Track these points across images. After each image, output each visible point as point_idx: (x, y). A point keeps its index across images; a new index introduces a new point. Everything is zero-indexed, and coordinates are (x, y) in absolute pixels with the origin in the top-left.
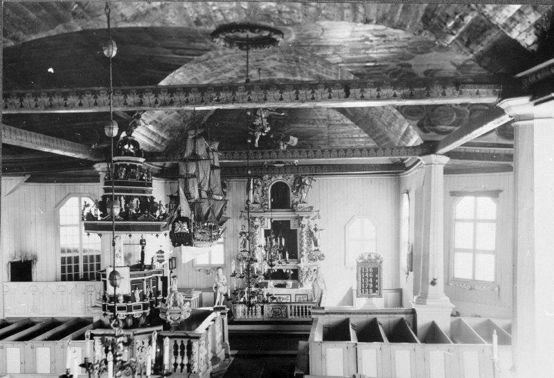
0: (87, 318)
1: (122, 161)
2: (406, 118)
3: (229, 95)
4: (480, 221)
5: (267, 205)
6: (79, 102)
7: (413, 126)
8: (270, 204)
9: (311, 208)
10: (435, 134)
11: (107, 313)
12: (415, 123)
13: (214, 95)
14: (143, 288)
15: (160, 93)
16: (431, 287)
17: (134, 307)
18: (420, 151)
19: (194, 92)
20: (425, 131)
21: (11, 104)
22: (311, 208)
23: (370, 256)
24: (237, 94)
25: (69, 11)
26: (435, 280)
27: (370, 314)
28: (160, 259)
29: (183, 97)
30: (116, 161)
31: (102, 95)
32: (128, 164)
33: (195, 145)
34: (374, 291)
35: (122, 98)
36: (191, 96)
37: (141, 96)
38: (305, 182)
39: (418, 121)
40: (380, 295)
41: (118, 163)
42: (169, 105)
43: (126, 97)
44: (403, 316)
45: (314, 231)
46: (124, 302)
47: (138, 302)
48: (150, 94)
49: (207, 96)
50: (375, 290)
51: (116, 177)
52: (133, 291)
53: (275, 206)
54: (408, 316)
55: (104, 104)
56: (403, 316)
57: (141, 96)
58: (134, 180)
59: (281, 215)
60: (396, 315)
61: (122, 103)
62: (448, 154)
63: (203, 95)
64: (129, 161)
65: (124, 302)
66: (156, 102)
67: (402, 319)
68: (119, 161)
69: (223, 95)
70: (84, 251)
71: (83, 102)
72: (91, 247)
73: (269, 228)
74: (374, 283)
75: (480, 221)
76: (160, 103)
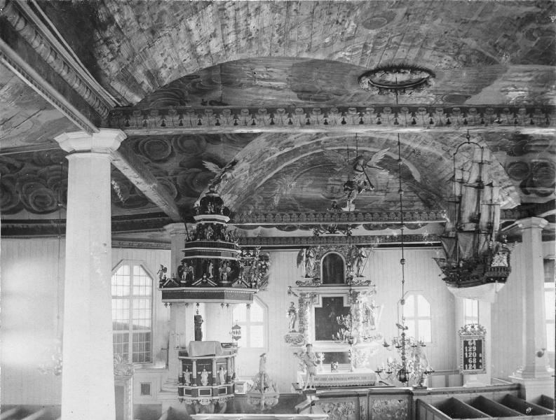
0: (148, 405)
1: (208, 220)
2: (510, 178)
3: (510, 117)
4: (420, 318)
5: (319, 279)
6: (341, 120)
7: (516, 186)
8: (322, 279)
9: (369, 282)
10: (536, 196)
11: (184, 398)
12: (518, 183)
13: (495, 116)
14: (211, 370)
15: (435, 112)
16: (537, 359)
17: (201, 391)
18: (517, 215)
19: (473, 112)
20: (526, 193)
21: (260, 120)
22: (369, 282)
23: (473, 327)
24: (519, 116)
25: (148, 29)
26: (544, 350)
27: (474, 392)
28: (236, 335)
29: (460, 118)
30: (200, 221)
31: (368, 113)
32: (215, 223)
33: (480, 171)
34: (478, 368)
35: (392, 116)
36: (470, 117)
37: (413, 115)
38: (361, 253)
39: (521, 182)
40: (484, 371)
41: (203, 223)
42: (445, 126)
43: (396, 116)
44: (508, 392)
45: (370, 308)
46: (208, 385)
47: (205, 387)
48: (424, 113)
49: (487, 117)
50: (478, 365)
51: (203, 237)
52: (199, 373)
53: (328, 281)
54: (513, 392)
55: (371, 123)
56: (508, 392)
57: (413, 115)
58: (205, 241)
59: (333, 291)
60: (501, 392)
61: (393, 123)
62: (546, 218)
63: (482, 116)
64: (215, 220)
65: (208, 385)
66: (431, 123)
67: (508, 395)
68: (204, 220)
69: (504, 118)
70: (135, 328)
71: (346, 120)
72: (142, 324)
73: (320, 306)
74: (478, 358)
75: (420, 318)
76: (435, 123)
